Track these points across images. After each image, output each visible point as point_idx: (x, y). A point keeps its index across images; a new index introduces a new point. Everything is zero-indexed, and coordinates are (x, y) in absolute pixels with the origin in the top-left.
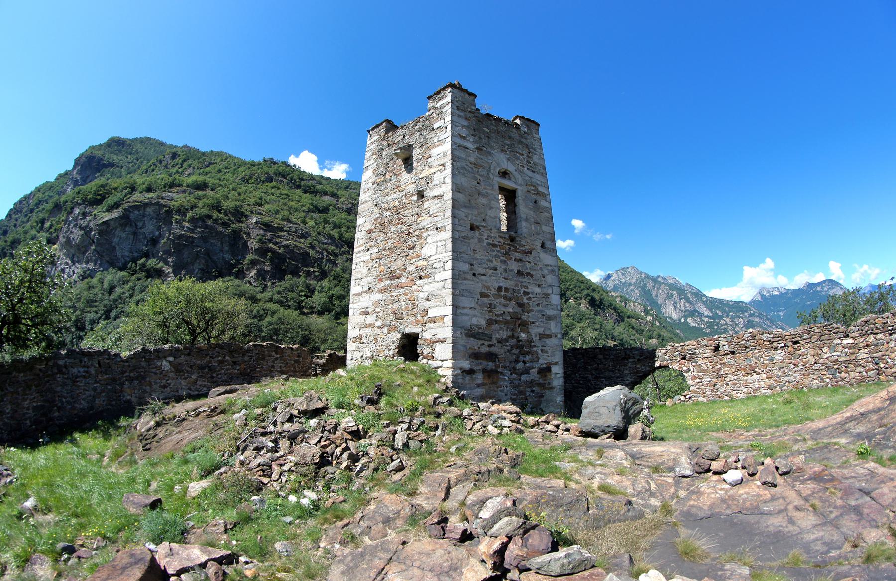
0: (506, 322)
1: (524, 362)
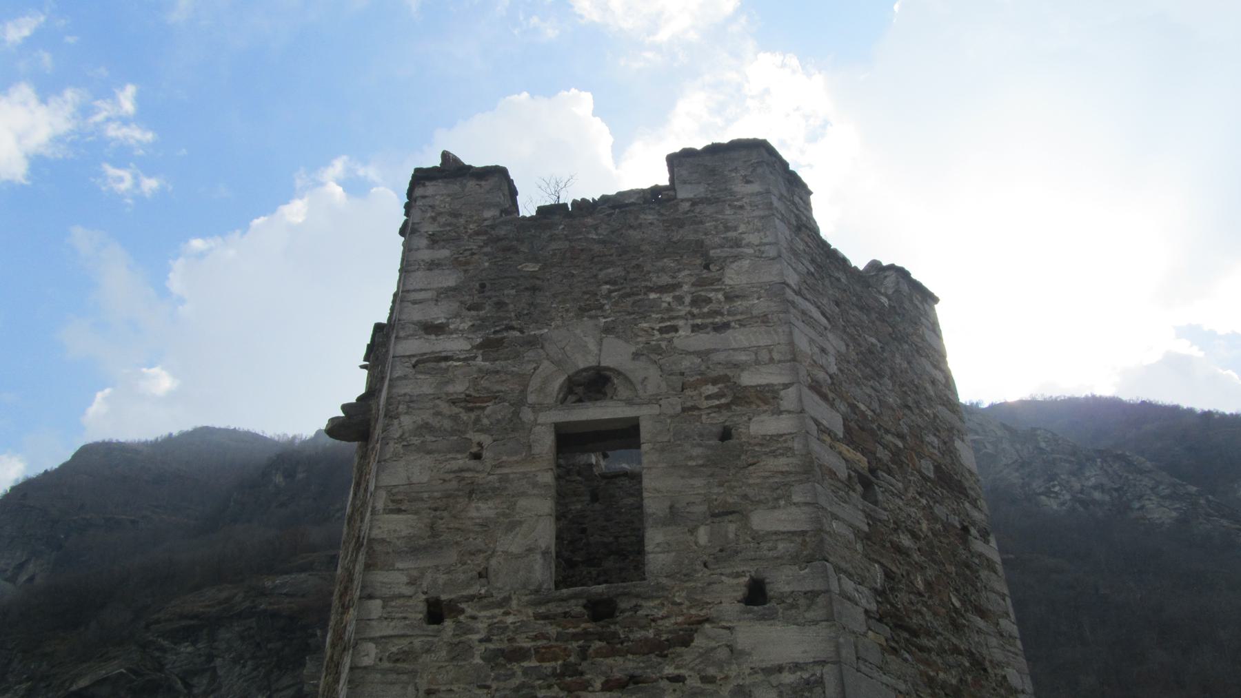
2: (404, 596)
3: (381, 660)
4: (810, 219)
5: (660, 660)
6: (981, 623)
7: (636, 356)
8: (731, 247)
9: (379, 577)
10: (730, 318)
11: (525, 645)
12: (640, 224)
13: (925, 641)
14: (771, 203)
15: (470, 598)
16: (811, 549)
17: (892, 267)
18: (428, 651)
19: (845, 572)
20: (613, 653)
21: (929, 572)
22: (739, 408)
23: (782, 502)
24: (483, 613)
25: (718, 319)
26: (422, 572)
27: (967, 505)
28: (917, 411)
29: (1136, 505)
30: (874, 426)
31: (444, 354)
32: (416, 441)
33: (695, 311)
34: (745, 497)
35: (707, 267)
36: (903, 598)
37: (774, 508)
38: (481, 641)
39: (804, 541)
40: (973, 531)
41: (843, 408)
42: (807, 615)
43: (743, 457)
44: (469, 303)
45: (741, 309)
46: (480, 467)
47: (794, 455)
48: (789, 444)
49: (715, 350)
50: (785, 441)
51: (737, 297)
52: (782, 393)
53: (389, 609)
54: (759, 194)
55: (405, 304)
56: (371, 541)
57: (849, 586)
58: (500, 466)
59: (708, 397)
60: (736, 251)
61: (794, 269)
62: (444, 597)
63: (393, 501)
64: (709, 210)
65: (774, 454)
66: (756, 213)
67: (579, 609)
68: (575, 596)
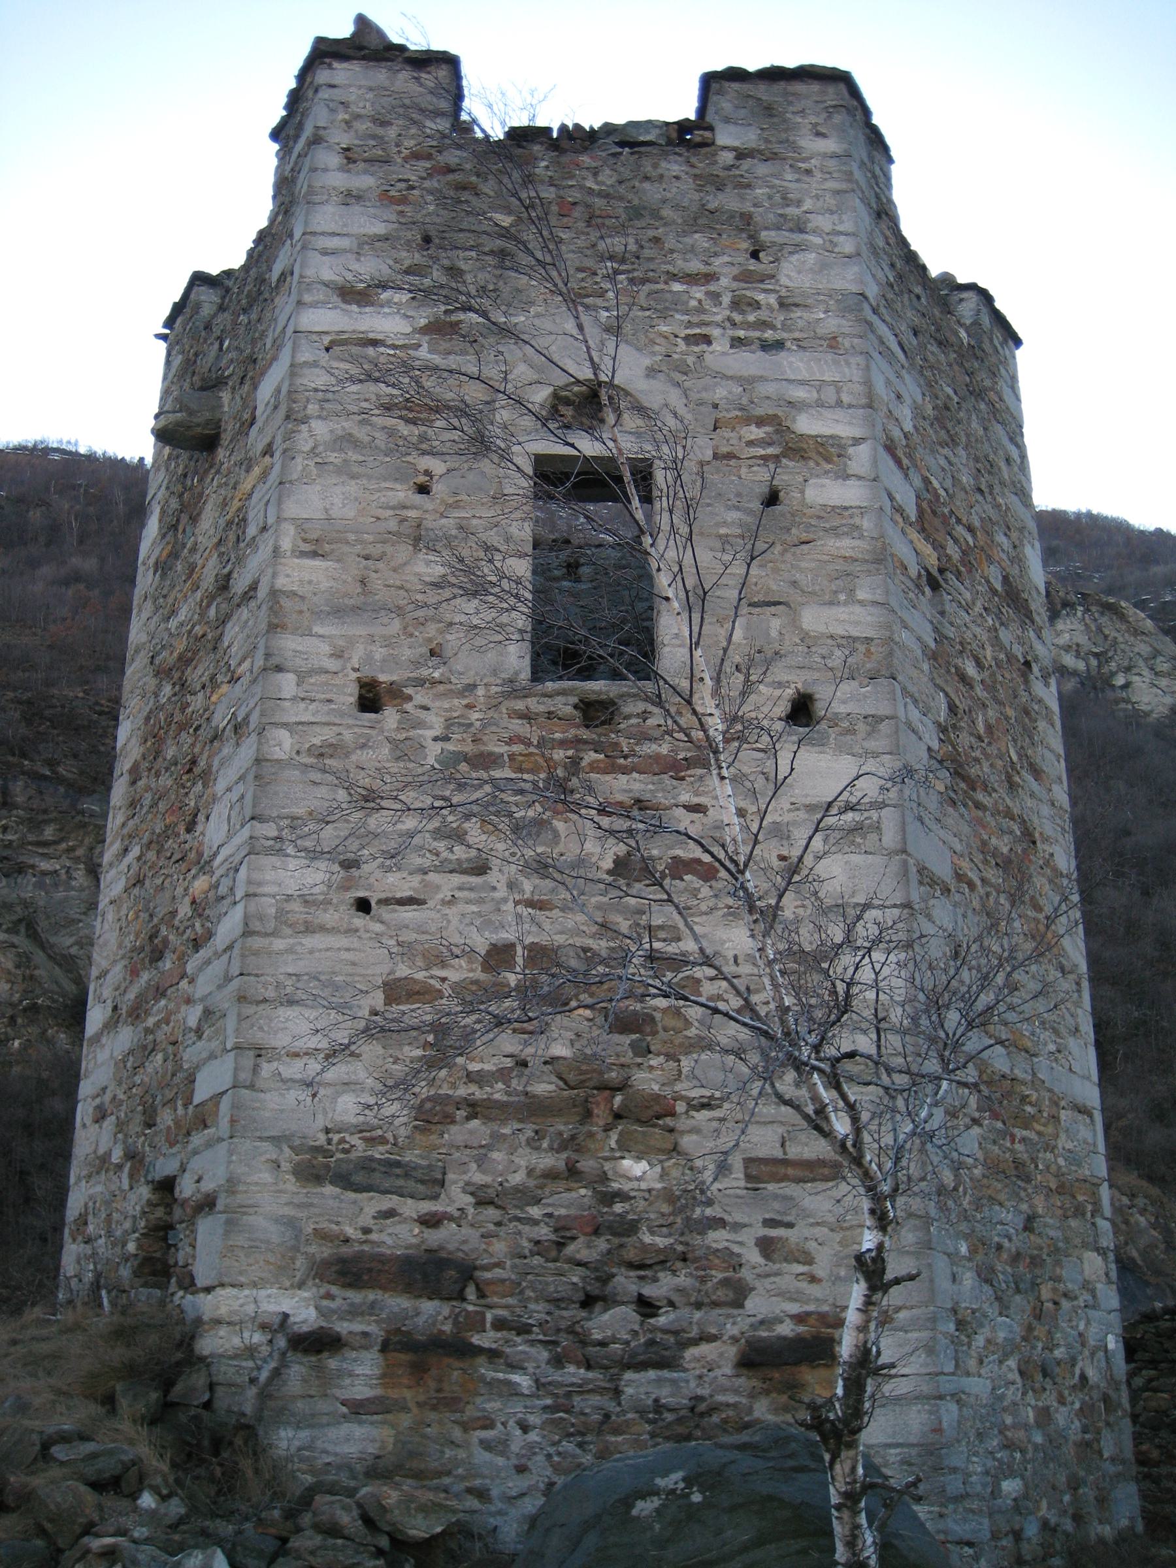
0: (534, 1109)
1: (646, 1307)
2: (327, 672)
3: (298, 752)
4: (890, 202)
5: (675, 782)
6: (1034, 785)
7: (651, 372)
8: (791, 230)
9: (289, 644)
10: (785, 335)
11: (497, 750)
12: (661, 176)
13: (980, 796)
14: (851, 173)
15: (420, 682)
16: (875, 664)
17: (973, 287)
18: (363, 746)
19: (912, 696)
20: (612, 768)
21: (990, 713)
22: (791, 464)
23: (842, 597)
24: (438, 704)
25: (769, 334)
26: (351, 641)
27: (1032, 634)
28: (989, 499)
29: (1120, 680)
30: (946, 511)
31: (371, 336)
32: (334, 457)
33: (738, 318)
34: (794, 583)
35: (755, 255)
36: (965, 740)
37: (831, 603)
38: (436, 739)
39: (868, 650)
40: (1035, 668)
41: (918, 482)
42: (866, 744)
43: (794, 531)
44: (407, 263)
45: (801, 324)
46: (430, 506)
47: (861, 537)
48: (857, 521)
49: (762, 379)
50: (851, 516)
51: (796, 305)
52: (851, 450)
53: (309, 688)
54: (835, 156)
55: (311, 254)
56: (274, 593)
57: (915, 714)
58: (456, 505)
59: (750, 443)
60: (798, 237)
61: (873, 276)
62: (382, 678)
63: (305, 540)
64: (762, 169)
65: (834, 531)
66: (831, 185)
67: (569, 710)
68: (563, 693)
